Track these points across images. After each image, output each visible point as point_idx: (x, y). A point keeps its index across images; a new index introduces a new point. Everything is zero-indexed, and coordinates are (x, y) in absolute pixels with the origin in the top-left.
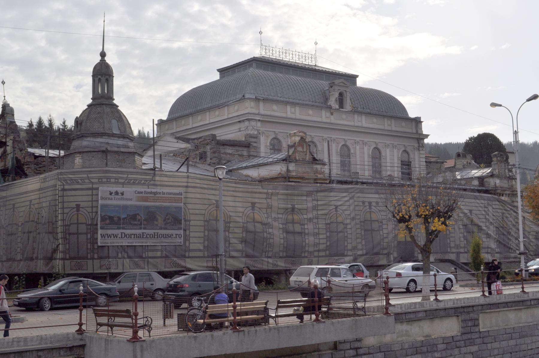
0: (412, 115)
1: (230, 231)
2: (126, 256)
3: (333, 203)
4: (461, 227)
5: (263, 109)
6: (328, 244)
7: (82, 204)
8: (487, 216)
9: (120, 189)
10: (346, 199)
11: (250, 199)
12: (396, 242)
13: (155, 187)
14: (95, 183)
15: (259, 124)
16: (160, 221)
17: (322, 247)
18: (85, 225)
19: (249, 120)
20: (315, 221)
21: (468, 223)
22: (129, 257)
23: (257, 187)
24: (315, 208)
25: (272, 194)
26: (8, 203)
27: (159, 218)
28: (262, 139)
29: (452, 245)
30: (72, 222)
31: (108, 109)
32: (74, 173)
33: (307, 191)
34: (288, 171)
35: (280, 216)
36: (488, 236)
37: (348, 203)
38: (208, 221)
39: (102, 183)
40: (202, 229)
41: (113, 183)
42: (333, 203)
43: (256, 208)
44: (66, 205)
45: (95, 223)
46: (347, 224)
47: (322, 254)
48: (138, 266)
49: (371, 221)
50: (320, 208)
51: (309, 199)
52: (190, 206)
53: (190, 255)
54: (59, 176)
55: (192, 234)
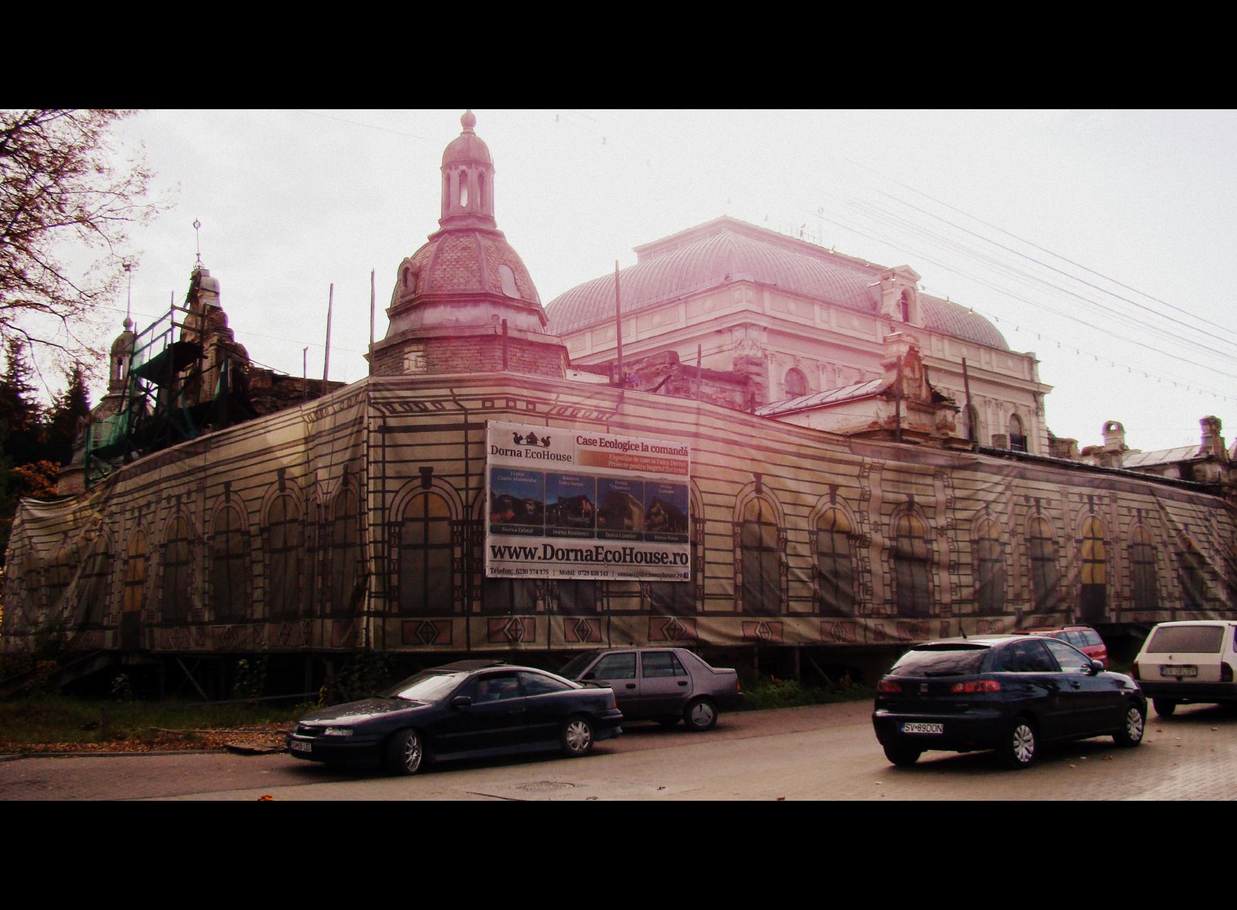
0: (1016, 344)
1: (788, 551)
2: (555, 608)
4: (1174, 557)
5: (770, 305)
6: (977, 585)
7: (438, 468)
9: (540, 430)
10: (1000, 489)
11: (827, 475)
12: (1079, 586)
13: (624, 431)
14: (475, 412)
15: (764, 337)
16: (637, 519)
17: (966, 592)
18: (446, 523)
19: (745, 326)
20: (951, 533)
22: (563, 611)
23: (841, 449)
24: (950, 505)
25: (872, 468)
26: (209, 482)
27: (635, 510)
28: (772, 368)
29: (1164, 594)
30: (409, 514)
31: (485, 242)
32: (413, 385)
33: (937, 466)
34: (896, 418)
35: (885, 520)
36: (1215, 576)
37: (1003, 499)
38: (743, 524)
39: (492, 410)
40: (729, 543)
41: (525, 413)
42: (981, 495)
43: (838, 499)
44: (390, 471)
45: (475, 517)
46: (1005, 544)
47: (967, 609)
48: (584, 635)
49: (1042, 539)
50: (958, 505)
51: (938, 483)
52: (703, 485)
53: (706, 609)
54: (371, 394)
55: (710, 556)
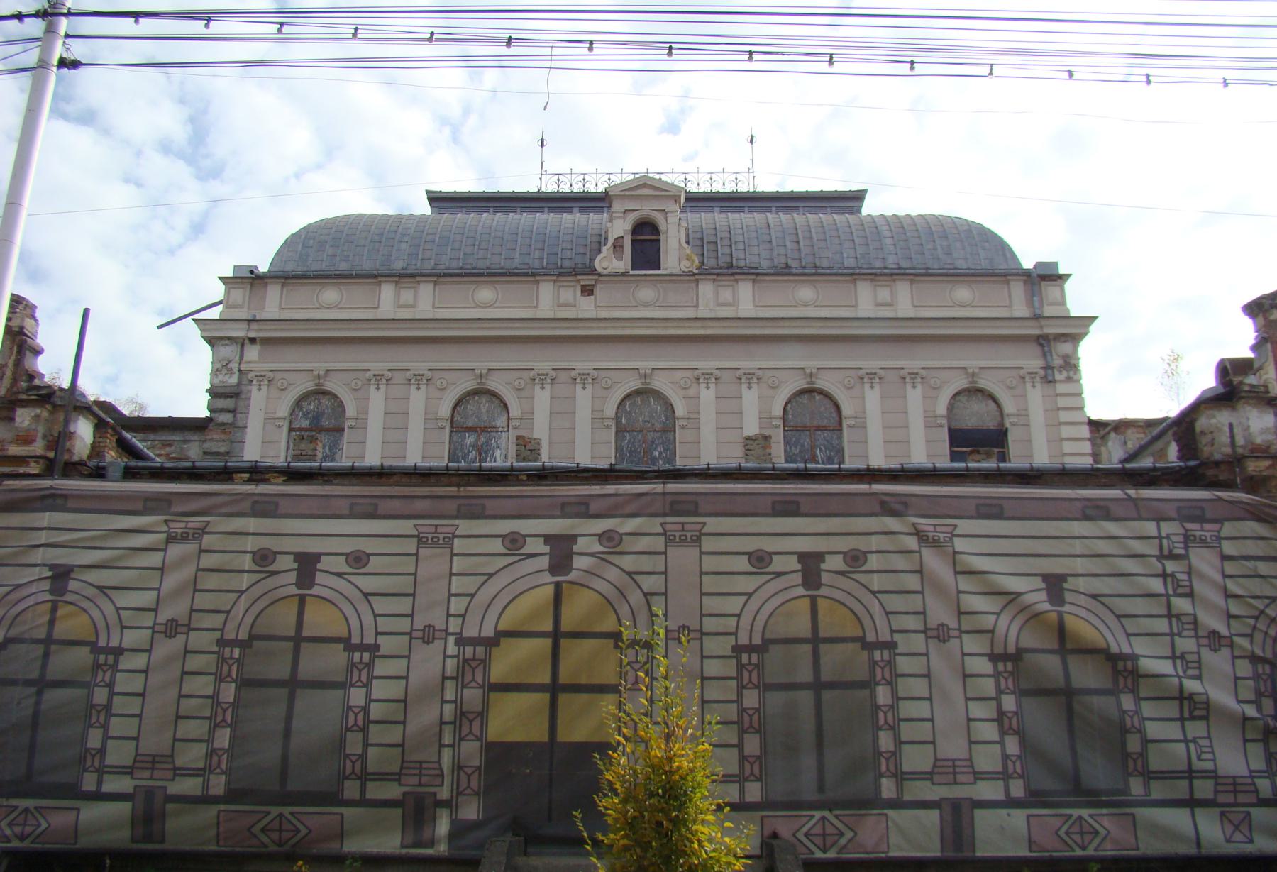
3: (38, 556)
8: (1182, 604)
21: (1028, 641)
29: (916, 759)
36: (1193, 708)
